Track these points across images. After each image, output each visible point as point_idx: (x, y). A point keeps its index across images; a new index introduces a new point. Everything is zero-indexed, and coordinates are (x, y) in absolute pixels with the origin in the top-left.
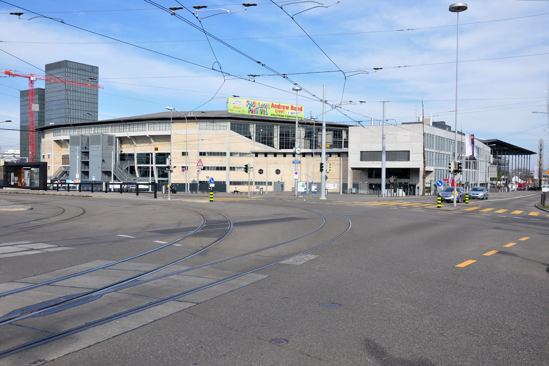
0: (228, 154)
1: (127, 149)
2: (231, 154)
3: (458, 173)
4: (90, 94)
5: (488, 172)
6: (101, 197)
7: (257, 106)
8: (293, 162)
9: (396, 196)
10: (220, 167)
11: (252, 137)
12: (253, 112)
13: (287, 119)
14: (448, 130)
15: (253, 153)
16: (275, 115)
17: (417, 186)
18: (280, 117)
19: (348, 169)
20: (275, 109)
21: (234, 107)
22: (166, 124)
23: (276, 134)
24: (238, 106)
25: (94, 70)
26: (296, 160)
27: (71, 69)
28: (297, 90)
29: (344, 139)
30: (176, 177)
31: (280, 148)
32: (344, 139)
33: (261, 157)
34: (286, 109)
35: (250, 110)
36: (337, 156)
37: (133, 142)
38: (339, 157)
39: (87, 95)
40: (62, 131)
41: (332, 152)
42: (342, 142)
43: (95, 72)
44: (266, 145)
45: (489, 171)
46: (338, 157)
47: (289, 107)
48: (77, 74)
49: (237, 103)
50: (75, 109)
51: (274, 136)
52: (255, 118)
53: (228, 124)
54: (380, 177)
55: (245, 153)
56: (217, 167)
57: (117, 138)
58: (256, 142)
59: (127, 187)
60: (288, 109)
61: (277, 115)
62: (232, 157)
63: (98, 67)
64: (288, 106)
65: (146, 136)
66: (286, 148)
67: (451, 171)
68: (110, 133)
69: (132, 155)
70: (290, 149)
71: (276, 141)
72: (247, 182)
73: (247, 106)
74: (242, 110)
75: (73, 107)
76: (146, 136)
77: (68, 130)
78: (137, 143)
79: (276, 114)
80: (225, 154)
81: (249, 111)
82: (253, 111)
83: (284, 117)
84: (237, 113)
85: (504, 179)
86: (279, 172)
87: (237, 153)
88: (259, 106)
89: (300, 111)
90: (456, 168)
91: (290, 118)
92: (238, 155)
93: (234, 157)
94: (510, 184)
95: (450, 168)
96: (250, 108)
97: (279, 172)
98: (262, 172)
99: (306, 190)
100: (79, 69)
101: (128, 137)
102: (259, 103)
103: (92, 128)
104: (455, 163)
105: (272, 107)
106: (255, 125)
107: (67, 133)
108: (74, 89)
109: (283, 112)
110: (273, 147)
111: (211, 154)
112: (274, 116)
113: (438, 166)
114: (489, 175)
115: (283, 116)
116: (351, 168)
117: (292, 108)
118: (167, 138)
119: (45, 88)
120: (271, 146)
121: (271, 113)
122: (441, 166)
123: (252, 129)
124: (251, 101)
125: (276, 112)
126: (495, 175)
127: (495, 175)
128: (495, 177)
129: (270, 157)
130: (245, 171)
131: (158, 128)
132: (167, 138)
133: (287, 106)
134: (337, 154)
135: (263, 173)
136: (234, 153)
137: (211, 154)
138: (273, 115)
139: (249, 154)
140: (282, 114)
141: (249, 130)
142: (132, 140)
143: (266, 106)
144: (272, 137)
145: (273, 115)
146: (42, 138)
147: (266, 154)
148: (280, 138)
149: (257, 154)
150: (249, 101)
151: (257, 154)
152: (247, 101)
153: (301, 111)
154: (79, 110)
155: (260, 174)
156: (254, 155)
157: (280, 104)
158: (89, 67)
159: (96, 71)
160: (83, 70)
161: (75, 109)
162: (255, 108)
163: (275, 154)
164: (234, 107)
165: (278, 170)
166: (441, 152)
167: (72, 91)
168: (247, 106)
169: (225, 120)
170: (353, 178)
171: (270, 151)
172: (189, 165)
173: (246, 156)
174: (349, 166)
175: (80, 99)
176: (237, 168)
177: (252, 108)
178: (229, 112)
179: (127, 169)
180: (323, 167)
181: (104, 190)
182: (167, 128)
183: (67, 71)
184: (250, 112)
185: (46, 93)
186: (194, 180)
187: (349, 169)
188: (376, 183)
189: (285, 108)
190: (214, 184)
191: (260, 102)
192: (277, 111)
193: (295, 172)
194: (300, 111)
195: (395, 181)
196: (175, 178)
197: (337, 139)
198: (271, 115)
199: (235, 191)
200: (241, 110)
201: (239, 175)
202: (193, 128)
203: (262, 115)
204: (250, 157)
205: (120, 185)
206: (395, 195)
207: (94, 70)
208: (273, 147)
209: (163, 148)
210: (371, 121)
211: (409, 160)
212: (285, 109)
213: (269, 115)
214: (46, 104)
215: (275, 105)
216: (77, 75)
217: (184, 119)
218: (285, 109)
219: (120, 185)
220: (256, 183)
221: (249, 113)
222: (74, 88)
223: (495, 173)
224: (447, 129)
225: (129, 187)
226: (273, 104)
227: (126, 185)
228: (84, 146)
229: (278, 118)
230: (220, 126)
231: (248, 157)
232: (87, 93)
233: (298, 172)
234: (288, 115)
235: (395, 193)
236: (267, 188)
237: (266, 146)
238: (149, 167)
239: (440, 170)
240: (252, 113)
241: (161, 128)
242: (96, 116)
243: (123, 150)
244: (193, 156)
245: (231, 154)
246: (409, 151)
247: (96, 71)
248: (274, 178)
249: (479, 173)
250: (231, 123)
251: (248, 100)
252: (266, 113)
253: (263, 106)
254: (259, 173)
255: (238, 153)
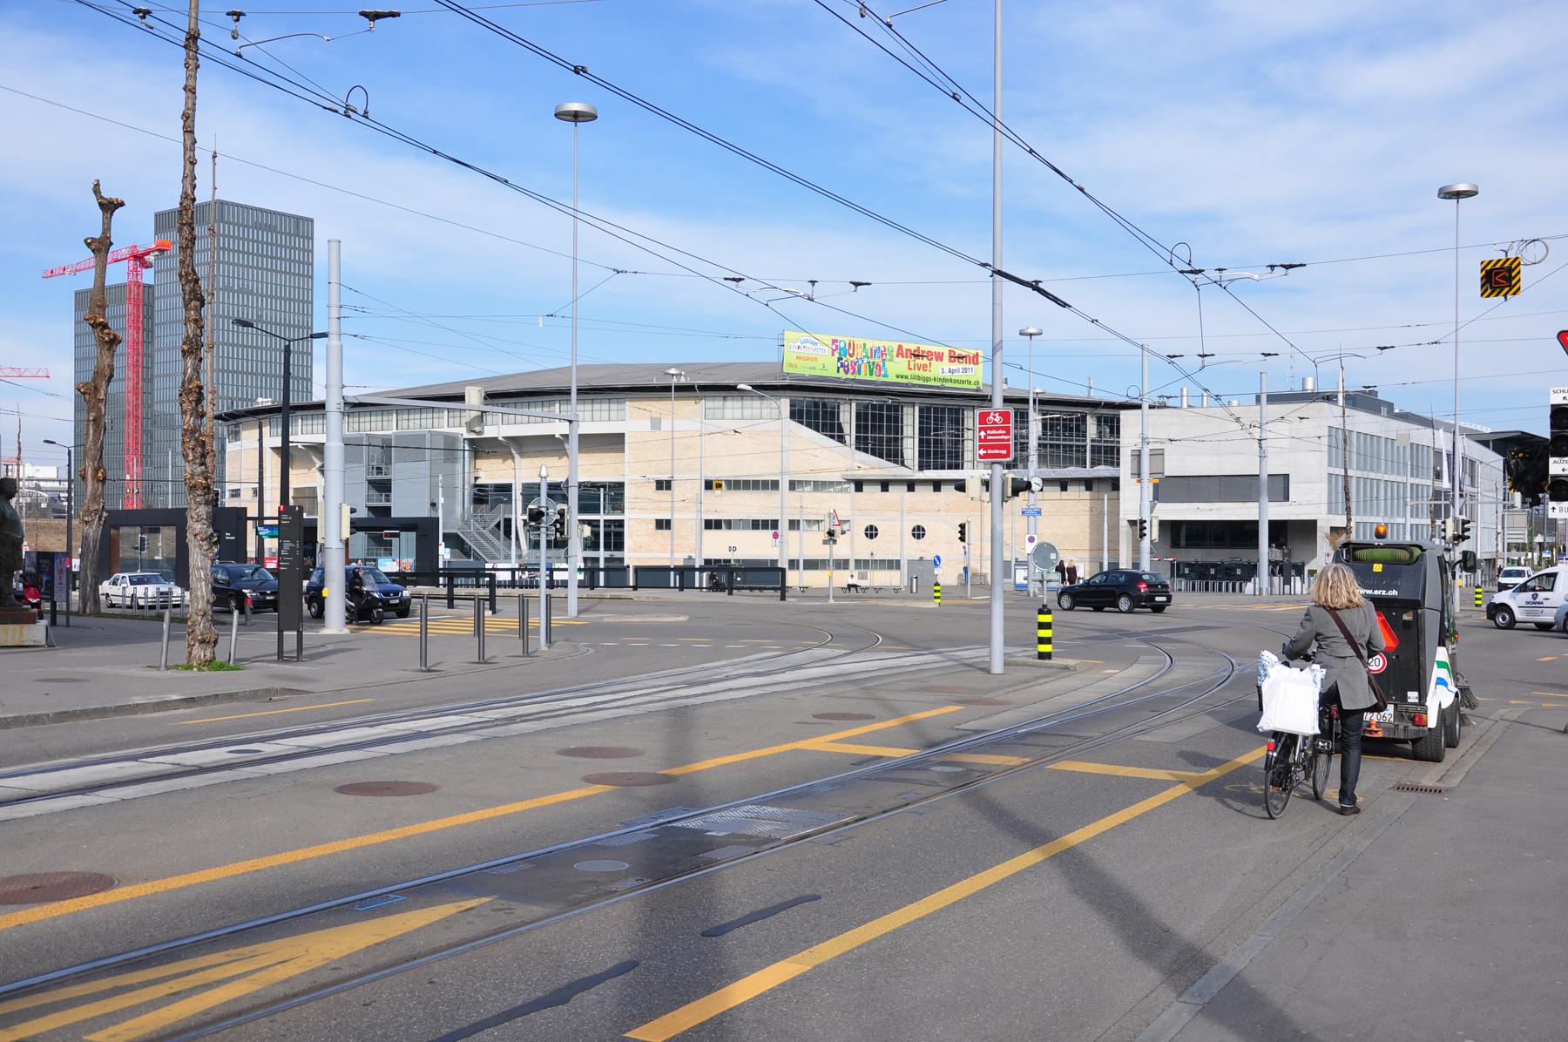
0: (784, 485)
1: (492, 472)
2: (793, 485)
3: (1463, 540)
4: (290, 300)
5: (1503, 528)
6: (659, 600)
7: (859, 353)
8: (1023, 513)
9: (1290, 594)
10: (762, 521)
11: (847, 438)
12: (848, 369)
13: (938, 387)
14: (1386, 415)
15: (849, 481)
16: (906, 377)
17: (1306, 569)
18: (921, 382)
19: (1121, 525)
20: (905, 361)
21: (798, 358)
22: (593, 403)
23: (910, 429)
24: (810, 353)
25: (301, 228)
26: (1032, 507)
27: (234, 225)
28: (1031, 335)
29: (1092, 441)
30: (640, 547)
31: (921, 468)
32: (1092, 441)
33: (873, 492)
34: (937, 360)
35: (842, 365)
36: (1083, 488)
37: (511, 454)
38: (1088, 492)
39: (281, 303)
40: (300, 421)
41: (1069, 477)
42: (1085, 446)
43: (303, 233)
44: (883, 458)
45: (1506, 526)
46: (1087, 490)
47: (943, 353)
48: (253, 240)
49: (808, 345)
50: (247, 346)
51: (905, 434)
52: (856, 386)
53: (785, 404)
54: (1254, 545)
55: (806, 481)
56: (753, 521)
57: (466, 441)
58: (858, 452)
59: (531, 578)
60: (941, 360)
61: (914, 377)
62: (794, 494)
63: (312, 220)
64: (941, 352)
65: (554, 435)
66: (950, 467)
67: (1447, 538)
68: (446, 429)
69: (506, 489)
70: (932, 471)
71: (911, 447)
72: (825, 560)
73: (833, 355)
74: (823, 365)
75: (269, 342)
76: (554, 435)
77: (307, 419)
78: (522, 455)
79: (909, 373)
80: (775, 485)
81: (838, 368)
82: (848, 366)
83: (932, 383)
84: (808, 373)
85: (1540, 544)
86: (874, 532)
87: (807, 483)
88: (864, 354)
89: (974, 364)
90: (1457, 531)
91: (947, 385)
92: (808, 489)
93: (801, 494)
94: (1565, 561)
95: (1444, 530)
96: (840, 359)
97: (874, 532)
98: (921, 532)
99: (1026, 582)
100: (258, 225)
101: (500, 438)
102: (865, 345)
103: (392, 415)
104: (1455, 520)
105: (898, 356)
106: (854, 405)
107: (315, 427)
108: (243, 285)
109: (928, 369)
110: (903, 464)
111: (735, 485)
112: (904, 381)
113: (1365, 514)
114: (1506, 537)
115: (927, 379)
116: (1129, 521)
117: (954, 358)
118: (614, 442)
119: (152, 283)
120: (896, 462)
121: (896, 371)
122: (1371, 514)
123: (848, 416)
124: (844, 340)
125: (910, 369)
126: (1522, 537)
127: (1522, 537)
128: (1522, 541)
129: (897, 492)
130: (960, 538)
131: (588, 415)
132: (614, 442)
133: (939, 353)
134: (1059, 483)
135: (876, 535)
136: (800, 482)
137: (735, 485)
138: (902, 377)
139: (839, 483)
140: (926, 374)
141: (838, 419)
142: (508, 447)
143: (883, 353)
144: (900, 436)
145: (902, 377)
146: (227, 440)
147: (885, 485)
148: (921, 441)
149: (859, 485)
150: (839, 338)
151: (859, 485)
152: (834, 341)
153: (976, 366)
154: (257, 347)
155: (869, 540)
156: (853, 486)
157: (919, 348)
158: (285, 220)
159: (308, 232)
160: (270, 229)
161: (247, 346)
162: (854, 359)
163: (911, 485)
164: (798, 358)
165: (919, 527)
166: (1372, 475)
167: (237, 291)
168: (833, 355)
169: (776, 393)
170: (1133, 547)
171: (895, 476)
172: (676, 519)
173: (832, 490)
174: (1121, 516)
175: (262, 315)
176: (808, 522)
177: (847, 359)
178: (786, 369)
179: (498, 526)
180: (1145, 528)
181: (631, 584)
182: (613, 414)
183: (221, 232)
184: (841, 369)
185: (158, 298)
186: (690, 558)
187: (1124, 524)
188: (1191, 560)
189: (934, 357)
190: (1381, 565)
191: (866, 343)
192: (912, 367)
193: (1028, 536)
194: (972, 366)
195: (1286, 559)
196: (640, 549)
197: (1072, 440)
198: (897, 377)
199: (850, 586)
200: (818, 365)
201: (809, 544)
202: (685, 415)
203: (874, 378)
204: (841, 491)
205: (510, 572)
206: (1287, 591)
207: (301, 228)
208: (903, 464)
209: (595, 468)
210: (1182, 396)
211: (1287, 498)
212: (934, 362)
213: (892, 378)
214: (157, 332)
215: (907, 350)
216: (241, 242)
217: (667, 389)
218: (934, 362)
219: (510, 572)
220: (858, 562)
221: (838, 372)
222: (243, 282)
223: (1522, 532)
224: (1384, 410)
225: (534, 577)
226: (900, 347)
227: (527, 572)
228: (375, 464)
229: (915, 385)
230: (771, 408)
231: (835, 491)
232: (271, 297)
233: (1035, 536)
234: (941, 375)
235: (1287, 587)
236: (801, 578)
237: (883, 462)
238: (599, 521)
239: (1361, 525)
240: (847, 372)
241: (597, 414)
242: (307, 366)
243: (480, 474)
244: (687, 487)
245: (793, 485)
246: (1287, 476)
247: (308, 232)
248: (913, 550)
249: (1479, 532)
250: (791, 400)
251: (834, 338)
252: (883, 373)
253: (874, 352)
254: (867, 535)
255: (810, 482)
